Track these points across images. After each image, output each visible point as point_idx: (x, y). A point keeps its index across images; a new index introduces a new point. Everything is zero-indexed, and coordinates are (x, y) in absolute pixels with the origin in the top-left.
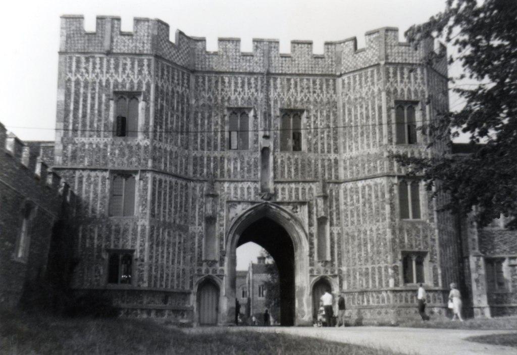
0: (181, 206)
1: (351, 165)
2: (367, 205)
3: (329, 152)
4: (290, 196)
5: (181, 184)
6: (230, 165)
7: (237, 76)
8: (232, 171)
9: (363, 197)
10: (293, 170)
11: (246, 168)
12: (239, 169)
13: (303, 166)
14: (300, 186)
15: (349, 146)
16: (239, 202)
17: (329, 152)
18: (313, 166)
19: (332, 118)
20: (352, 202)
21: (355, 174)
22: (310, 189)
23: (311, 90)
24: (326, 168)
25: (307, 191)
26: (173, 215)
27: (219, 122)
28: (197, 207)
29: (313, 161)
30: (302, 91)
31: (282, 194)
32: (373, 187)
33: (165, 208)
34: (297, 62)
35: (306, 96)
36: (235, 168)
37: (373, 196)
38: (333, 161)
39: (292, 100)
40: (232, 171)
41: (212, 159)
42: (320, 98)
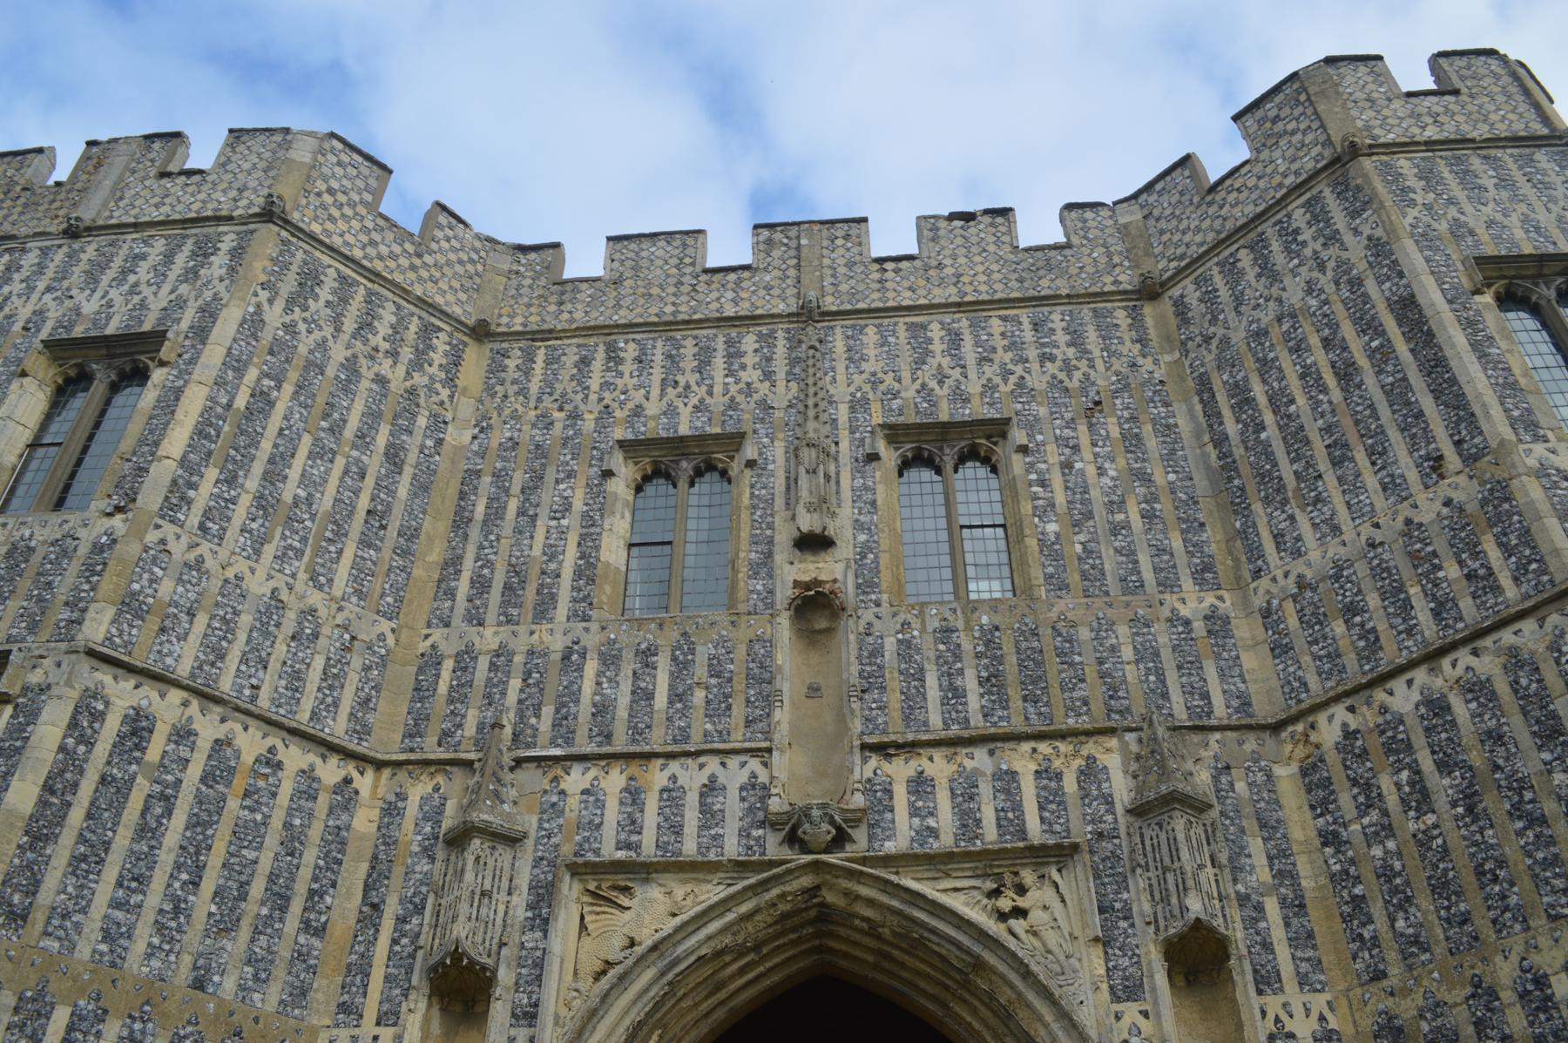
0: (279, 900)
1: (1314, 620)
2: (1495, 804)
3: (1168, 583)
4: (968, 821)
5: (308, 774)
6: (614, 682)
7: (678, 335)
8: (622, 713)
9: (1444, 767)
10: (970, 683)
11: (699, 696)
12: (661, 700)
13: (1032, 664)
14: (1023, 761)
15: (1278, 538)
16: (645, 871)
17: (1168, 583)
18: (1085, 659)
19: (1152, 443)
20: (1374, 816)
21: (1350, 660)
22: (1091, 772)
23: (1032, 353)
24: (1168, 660)
25: (1070, 784)
26: (193, 937)
27: (578, 505)
28: (392, 908)
29: (1084, 634)
30: (983, 360)
31: (914, 812)
32: (1502, 687)
33: (134, 879)
34: (949, 271)
35: (1006, 374)
36: (643, 695)
37: (1519, 728)
38: (1199, 626)
39: (942, 392)
40: (622, 713)
41: (519, 659)
42: (1078, 375)
